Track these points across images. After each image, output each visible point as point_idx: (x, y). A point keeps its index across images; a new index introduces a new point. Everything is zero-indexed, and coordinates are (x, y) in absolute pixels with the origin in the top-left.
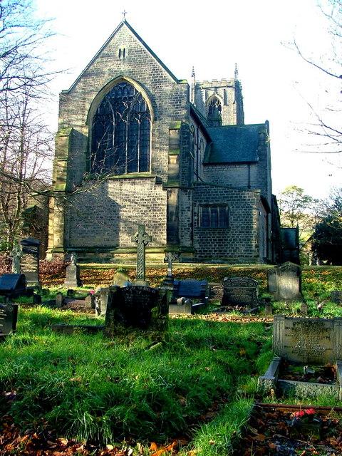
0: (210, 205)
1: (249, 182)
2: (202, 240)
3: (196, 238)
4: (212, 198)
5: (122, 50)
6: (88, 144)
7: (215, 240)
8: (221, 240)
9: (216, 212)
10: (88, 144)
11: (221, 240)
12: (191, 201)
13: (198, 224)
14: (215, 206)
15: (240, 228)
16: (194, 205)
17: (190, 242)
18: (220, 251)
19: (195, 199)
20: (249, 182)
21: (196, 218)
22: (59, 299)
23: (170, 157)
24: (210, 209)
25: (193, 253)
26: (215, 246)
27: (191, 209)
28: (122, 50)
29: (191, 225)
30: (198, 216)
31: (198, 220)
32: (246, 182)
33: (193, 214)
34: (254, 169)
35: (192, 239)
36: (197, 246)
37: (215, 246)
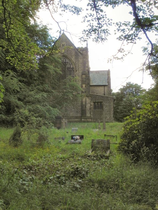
0: (96, 102)
1: (104, 92)
2: (94, 114)
3: (92, 113)
4: (97, 99)
5: (63, 44)
6: (24, 85)
7: (98, 114)
8: (101, 114)
9: (98, 104)
10: (24, 85)
11: (101, 114)
12: (90, 101)
13: (92, 108)
14: (98, 102)
15: (107, 110)
16: (91, 102)
17: (90, 115)
18: (100, 118)
19: (91, 100)
20: (104, 92)
21: (91, 106)
22: (71, 199)
23: (107, 84)
24: (99, 103)
25: (91, 119)
26: (98, 116)
27: (90, 103)
28: (63, 44)
29: (90, 109)
30: (92, 106)
31: (92, 107)
32: (103, 92)
33: (91, 105)
34: (106, 88)
35: (90, 114)
36: (92, 116)
37: (98, 116)
